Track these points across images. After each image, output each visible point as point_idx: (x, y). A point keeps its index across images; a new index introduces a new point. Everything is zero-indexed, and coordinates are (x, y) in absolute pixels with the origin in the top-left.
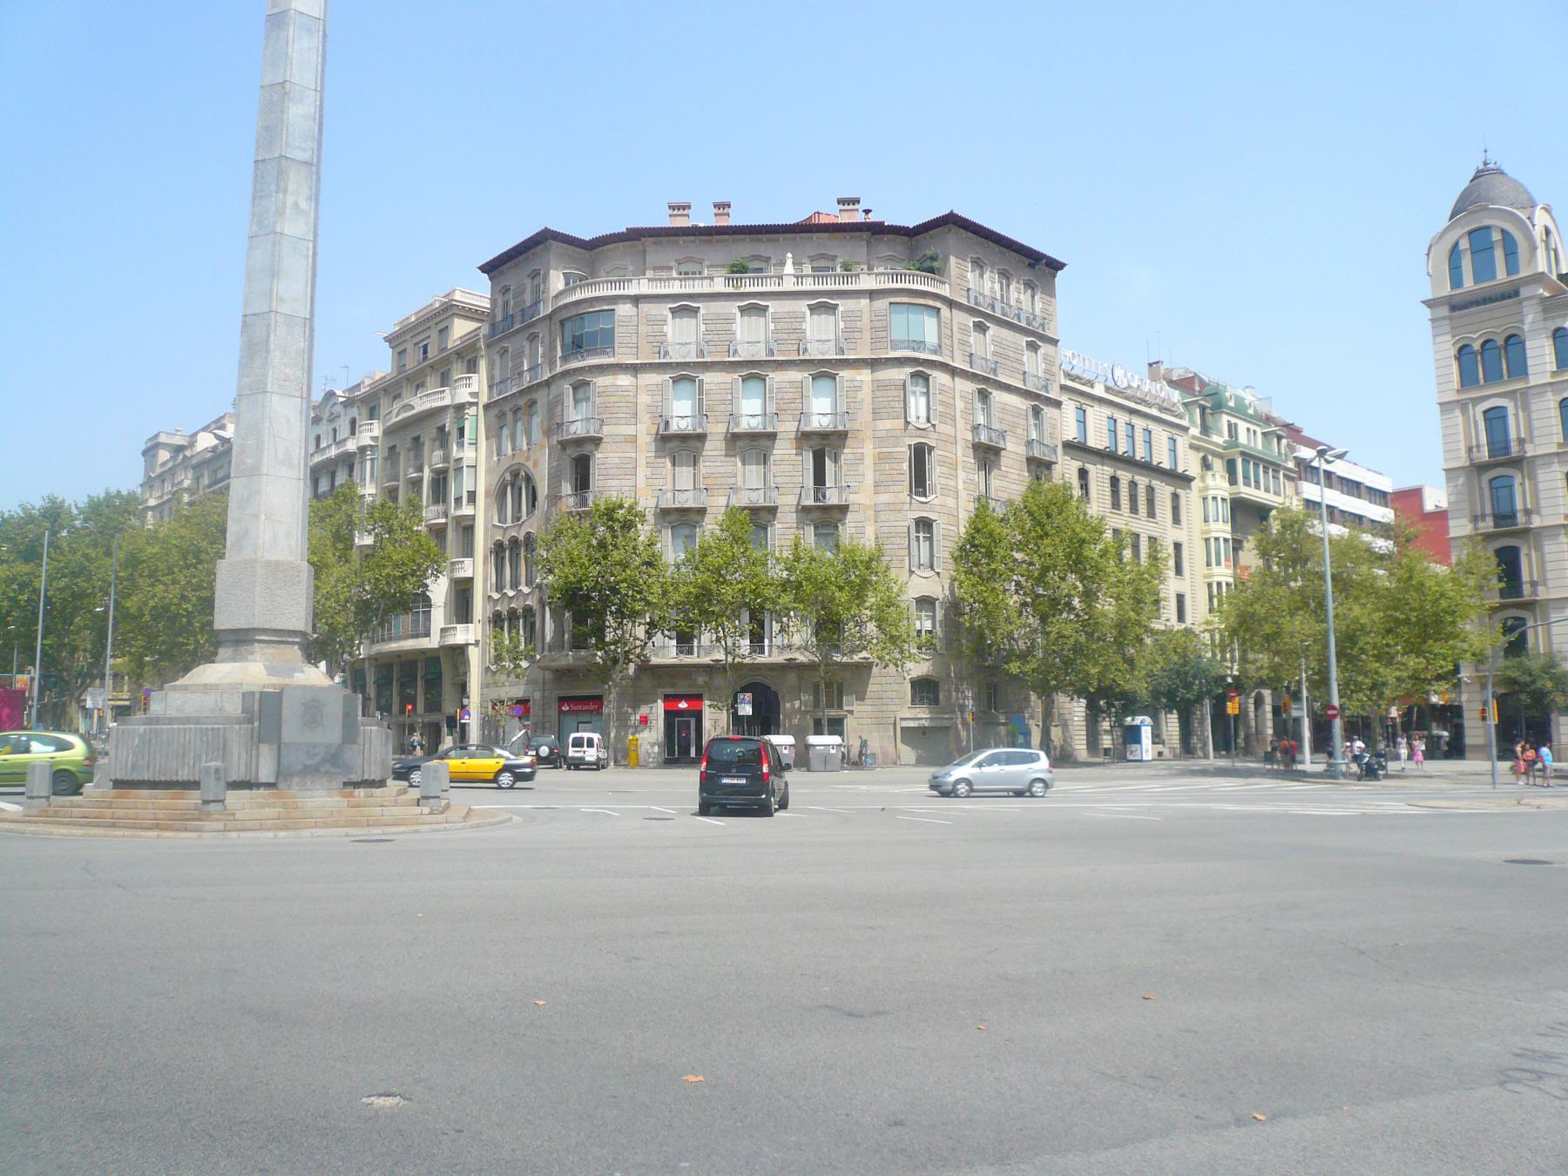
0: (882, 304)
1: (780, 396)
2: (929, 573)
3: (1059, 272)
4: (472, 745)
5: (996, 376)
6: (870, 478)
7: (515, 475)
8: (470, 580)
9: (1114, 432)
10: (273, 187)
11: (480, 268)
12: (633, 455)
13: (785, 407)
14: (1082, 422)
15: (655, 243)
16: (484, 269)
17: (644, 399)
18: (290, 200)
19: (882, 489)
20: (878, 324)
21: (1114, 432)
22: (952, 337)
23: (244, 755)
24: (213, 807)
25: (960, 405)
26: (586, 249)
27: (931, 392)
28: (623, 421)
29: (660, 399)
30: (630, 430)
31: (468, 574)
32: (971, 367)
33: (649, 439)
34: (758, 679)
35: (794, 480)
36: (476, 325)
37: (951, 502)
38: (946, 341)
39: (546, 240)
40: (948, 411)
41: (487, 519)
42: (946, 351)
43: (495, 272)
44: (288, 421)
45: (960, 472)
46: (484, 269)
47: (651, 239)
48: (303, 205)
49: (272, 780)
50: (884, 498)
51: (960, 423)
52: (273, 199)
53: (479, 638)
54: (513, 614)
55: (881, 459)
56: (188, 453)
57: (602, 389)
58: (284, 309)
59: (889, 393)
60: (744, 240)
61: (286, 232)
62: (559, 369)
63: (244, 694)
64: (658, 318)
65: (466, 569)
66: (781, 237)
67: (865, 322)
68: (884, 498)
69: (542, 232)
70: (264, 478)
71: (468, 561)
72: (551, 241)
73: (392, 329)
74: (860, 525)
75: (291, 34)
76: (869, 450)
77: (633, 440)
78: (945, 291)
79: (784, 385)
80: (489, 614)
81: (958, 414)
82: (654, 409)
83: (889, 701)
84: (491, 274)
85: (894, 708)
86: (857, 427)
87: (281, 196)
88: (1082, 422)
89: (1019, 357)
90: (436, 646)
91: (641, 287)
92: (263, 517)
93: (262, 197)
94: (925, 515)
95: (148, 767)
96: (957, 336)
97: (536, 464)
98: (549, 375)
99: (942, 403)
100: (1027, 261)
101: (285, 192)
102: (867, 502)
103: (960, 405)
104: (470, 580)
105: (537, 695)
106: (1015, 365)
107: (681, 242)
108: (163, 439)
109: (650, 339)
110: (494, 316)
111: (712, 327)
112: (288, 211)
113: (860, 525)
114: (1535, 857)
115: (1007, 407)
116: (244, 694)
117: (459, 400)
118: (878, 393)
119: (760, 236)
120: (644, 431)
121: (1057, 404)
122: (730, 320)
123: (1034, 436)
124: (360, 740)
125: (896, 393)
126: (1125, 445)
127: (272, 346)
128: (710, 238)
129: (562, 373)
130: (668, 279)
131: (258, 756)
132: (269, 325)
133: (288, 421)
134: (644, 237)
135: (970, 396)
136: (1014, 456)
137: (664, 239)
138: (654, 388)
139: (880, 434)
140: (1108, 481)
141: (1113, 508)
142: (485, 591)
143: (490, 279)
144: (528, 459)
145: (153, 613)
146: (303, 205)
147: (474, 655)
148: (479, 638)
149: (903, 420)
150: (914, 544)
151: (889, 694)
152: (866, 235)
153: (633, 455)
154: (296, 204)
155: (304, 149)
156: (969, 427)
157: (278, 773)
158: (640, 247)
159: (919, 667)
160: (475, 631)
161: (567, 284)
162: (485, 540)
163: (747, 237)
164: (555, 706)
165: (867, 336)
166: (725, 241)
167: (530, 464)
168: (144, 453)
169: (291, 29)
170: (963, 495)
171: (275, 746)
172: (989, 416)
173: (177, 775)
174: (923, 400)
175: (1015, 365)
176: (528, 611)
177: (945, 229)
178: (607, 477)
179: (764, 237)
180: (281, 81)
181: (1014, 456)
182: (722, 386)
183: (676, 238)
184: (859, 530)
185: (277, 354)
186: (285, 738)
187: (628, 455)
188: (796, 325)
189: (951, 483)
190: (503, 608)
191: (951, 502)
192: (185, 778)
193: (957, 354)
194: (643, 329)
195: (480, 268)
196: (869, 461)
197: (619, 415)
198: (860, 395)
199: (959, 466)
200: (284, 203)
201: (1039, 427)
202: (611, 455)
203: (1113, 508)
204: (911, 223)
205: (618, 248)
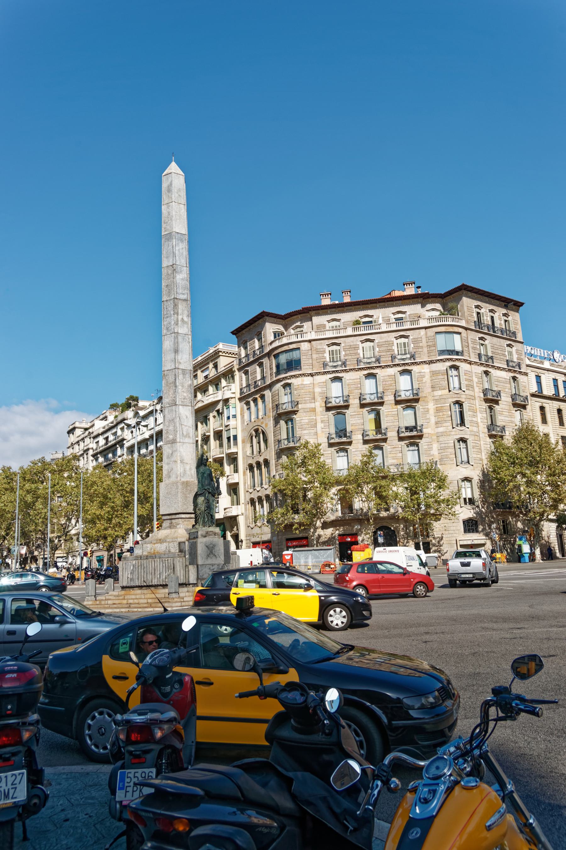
0: (431, 332)
1: (384, 383)
2: (468, 465)
3: (521, 308)
4: (551, 521)
5: (520, 369)
6: (433, 420)
7: (256, 431)
8: (237, 484)
9: (556, 386)
10: (172, 312)
12: (315, 418)
13: (387, 388)
14: (539, 383)
16: (233, 333)
17: (318, 390)
18: (180, 317)
19: (440, 425)
20: (430, 344)
21: (556, 386)
22: (468, 346)
23: (182, 571)
24: (174, 595)
25: (475, 380)
26: (282, 319)
27: (461, 375)
28: (308, 402)
29: (325, 389)
30: (312, 405)
31: (236, 481)
32: (520, 369)
33: (321, 409)
34: (385, 524)
35: (395, 424)
36: (231, 360)
37: (475, 429)
38: (465, 349)
39: (264, 316)
40: (470, 383)
41: (244, 453)
42: (465, 353)
43: (240, 334)
44: (187, 417)
45: (478, 413)
46: (233, 333)
47: (314, 312)
48: (186, 319)
49: (195, 582)
50: (441, 430)
51: (477, 389)
52: (173, 318)
53: (243, 512)
54: (260, 499)
55: (438, 410)
56: (91, 430)
57: (297, 387)
58: (181, 367)
59: (439, 377)
61: (179, 332)
62: (275, 379)
63: (179, 543)
64: (321, 350)
65: (235, 478)
67: (424, 343)
68: (441, 430)
69: (262, 313)
70: (178, 444)
71: (236, 474)
72: (266, 317)
74: (429, 444)
75: (174, 243)
76: (431, 406)
77: (314, 410)
78: (463, 323)
79: (386, 378)
80: (248, 499)
81: (475, 385)
82: (323, 395)
83: (452, 532)
85: (455, 535)
86: (424, 395)
87: (176, 316)
88: (539, 383)
89: (503, 353)
90: (222, 517)
92: (179, 462)
93: (167, 317)
94: (462, 436)
95: (138, 579)
96: (471, 345)
97: (266, 425)
98: (270, 382)
99: (466, 380)
100: (503, 304)
101: (178, 314)
102: (433, 432)
103: (475, 380)
104: (237, 484)
105: (275, 538)
106: (502, 357)
108: (77, 425)
109: (318, 361)
110: (240, 355)
111: (348, 352)
112: (180, 322)
113: (429, 444)
115: (500, 379)
116: (179, 543)
117: (226, 397)
118: (434, 378)
120: (319, 405)
121: (526, 374)
122: (356, 348)
123: (486, 386)
124: (231, 562)
125: (442, 377)
126: (564, 392)
127: (178, 384)
129: (277, 380)
131: (189, 571)
132: (175, 375)
133: (187, 417)
134: (311, 311)
135: (480, 375)
136: (505, 403)
138: (322, 384)
139: (436, 398)
140: (556, 412)
141: (560, 425)
142: (245, 488)
143: (237, 337)
144: (262, 423)
146: (186, 319)
147: (241, 521)
148: (243, 512)
149: (448, 390)
150: (458, 451)
151: (452, 528)
152: (420, 300)
153: (315, 418)
154: (183, 319)
155: (184, 294)
156: (481, 391)
157: (198, 579)
159: (467, 513)
160: (241, 509)
161: (275, 337)
162: (244, 463)
164: (285, 543)
165: (425, 350)
166: (351, 309)
167: (263, 425)
169: (174, 240)
170: (481, 425)
171: (195, 566)
172: (491, 384)
173: (152, 582)
174: (456, 379)
175: (502, 357)
176: (267, 496)
177: (460, 292)
178: (302, 429)
180: (172, 264)
181: (505, 403)
182: (355, 381)
183: (326, 310)
184: (430, 446)
185: (180, 387)
186: (200, 562)
187: (312, 418)
188: (390, 348)
189: (474, 419)
190: (255, 496)
191: (475, 429)
192: (156, 583)
193: (472, 355)
194: (315, 356)
196: (432, 411)
197: (306, 399)
198: (424, 379)
199: (478, 411)
200: (177, 319)
201: (490, 382)
202: (304, 418)
203: (560, 425)
204: (443, 292)
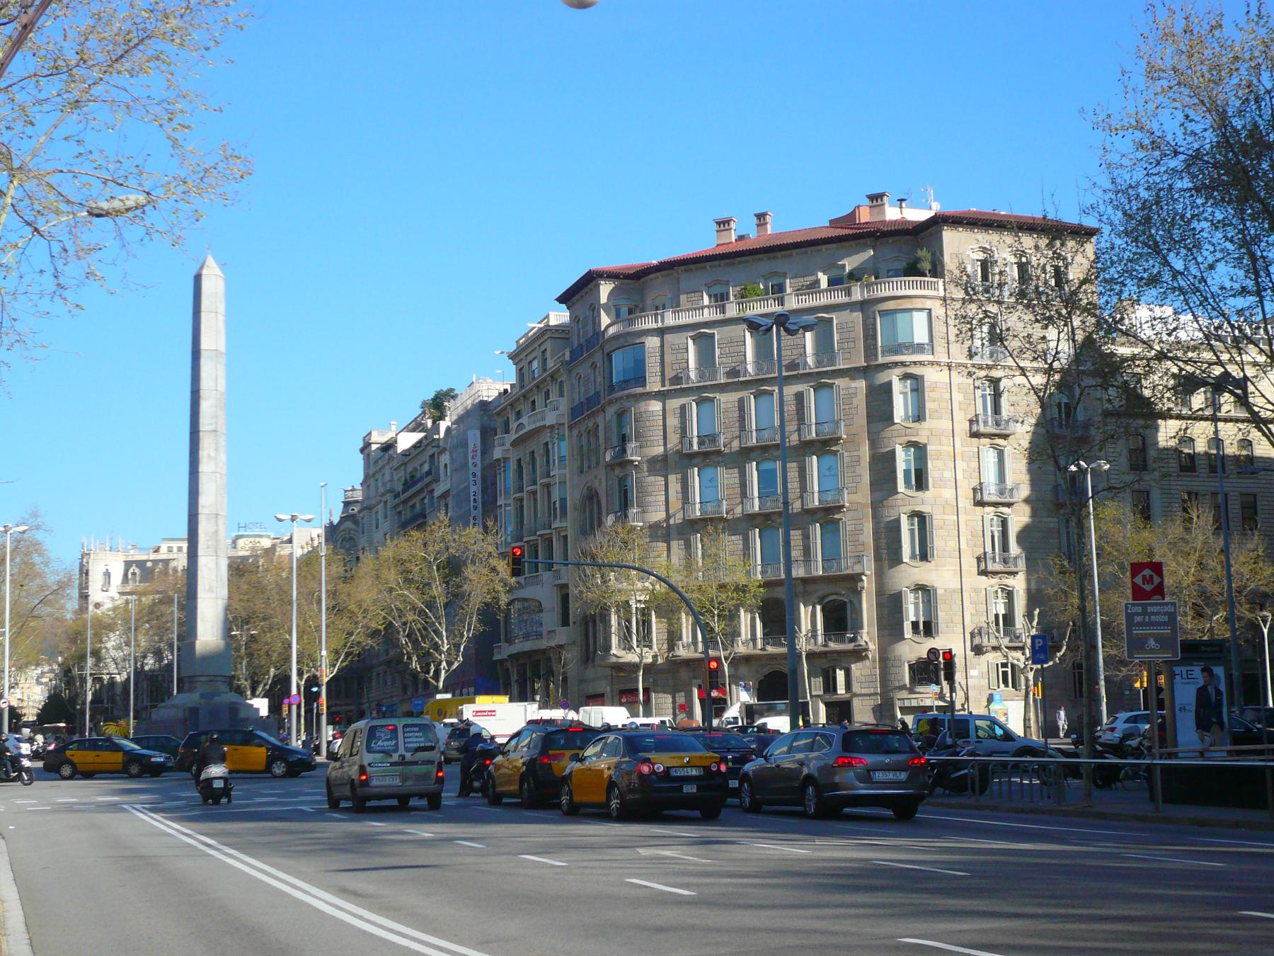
11: (557, 300)
15: (686, 271)
39: (594, 279)
60: (761, 259)
66: (794, 252)
73: (512, 347)
84: (569, 303)
91: (670, 319)
107: (794, 254)
114: (400, 864)
119: (775, 254)
128: (732, 261)
130: (1190, 308)
137: (693, 267)
145: (160, 678)
158: (676, 275)
163: (750, 258)
166: (747, 262)
168: (362, 451)
179: (780, 254)
195: (557, 300)
205: (821, 250)
